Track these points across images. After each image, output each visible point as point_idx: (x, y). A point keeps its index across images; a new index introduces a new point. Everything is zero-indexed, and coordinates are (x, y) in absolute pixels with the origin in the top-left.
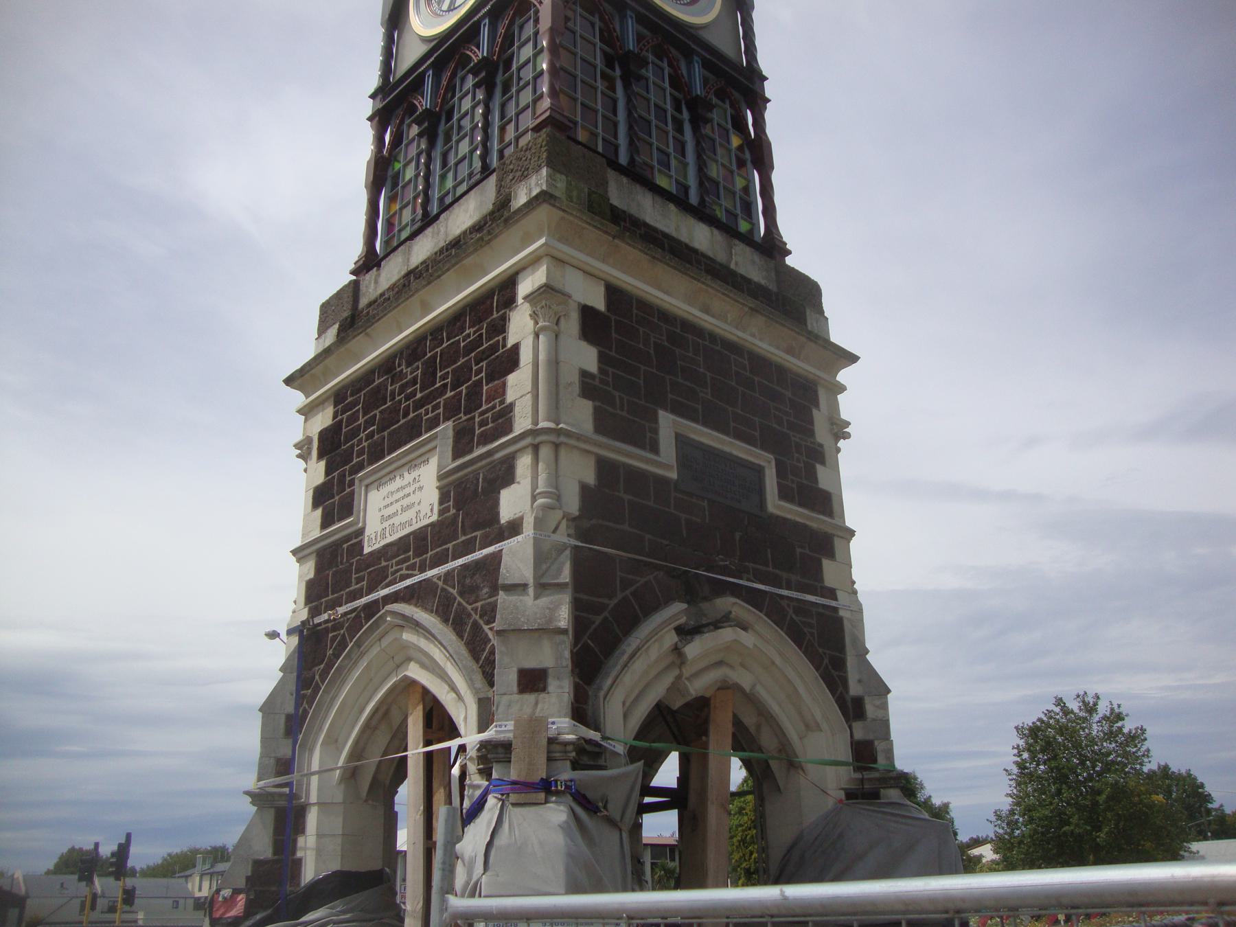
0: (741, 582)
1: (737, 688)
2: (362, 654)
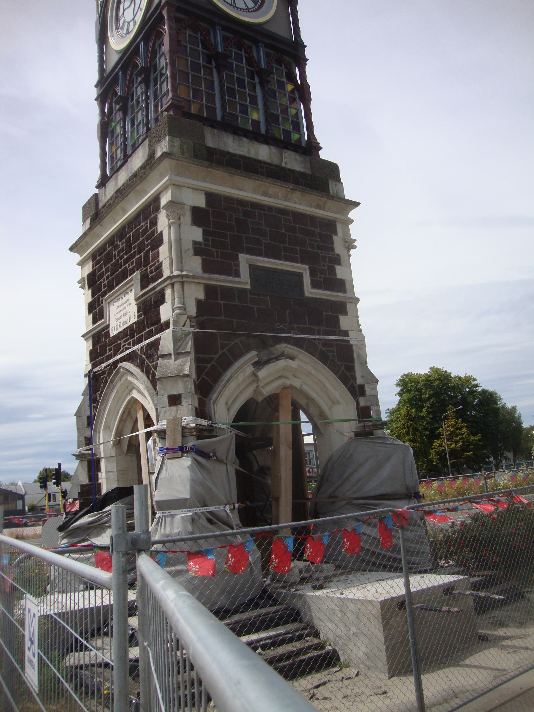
0: (289, 335)
1: (291, 387)
2: (114, 386)
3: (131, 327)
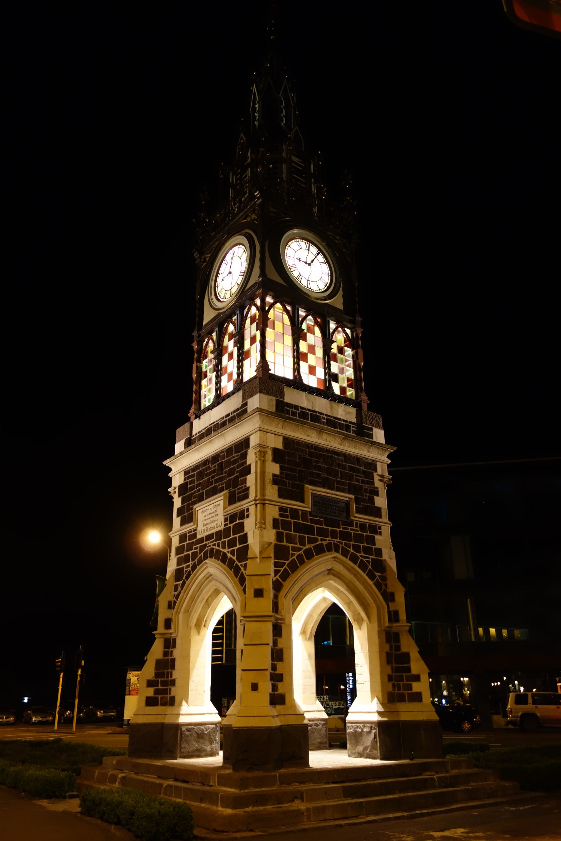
3: (218, 533)
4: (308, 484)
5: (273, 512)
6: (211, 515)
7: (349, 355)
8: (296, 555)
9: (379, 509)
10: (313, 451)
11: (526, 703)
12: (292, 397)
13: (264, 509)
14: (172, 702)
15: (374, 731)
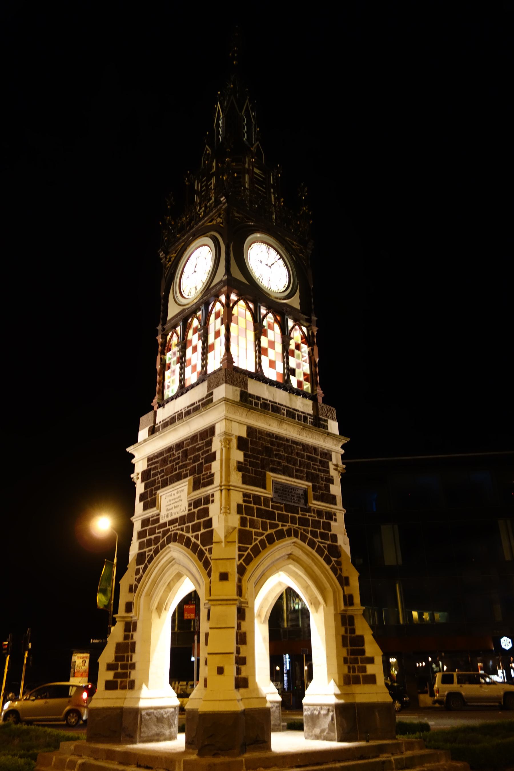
4: (269, 471)
5: (237, 498)
6: (174, 500)
7: (305, 352)
8: (259, 540)
9: (334, 497)
10: (274, 440)
11: (452, 682)
12: (254, 388)
13: (228, 496)
14: (132, 685)
15: (331, 714)
